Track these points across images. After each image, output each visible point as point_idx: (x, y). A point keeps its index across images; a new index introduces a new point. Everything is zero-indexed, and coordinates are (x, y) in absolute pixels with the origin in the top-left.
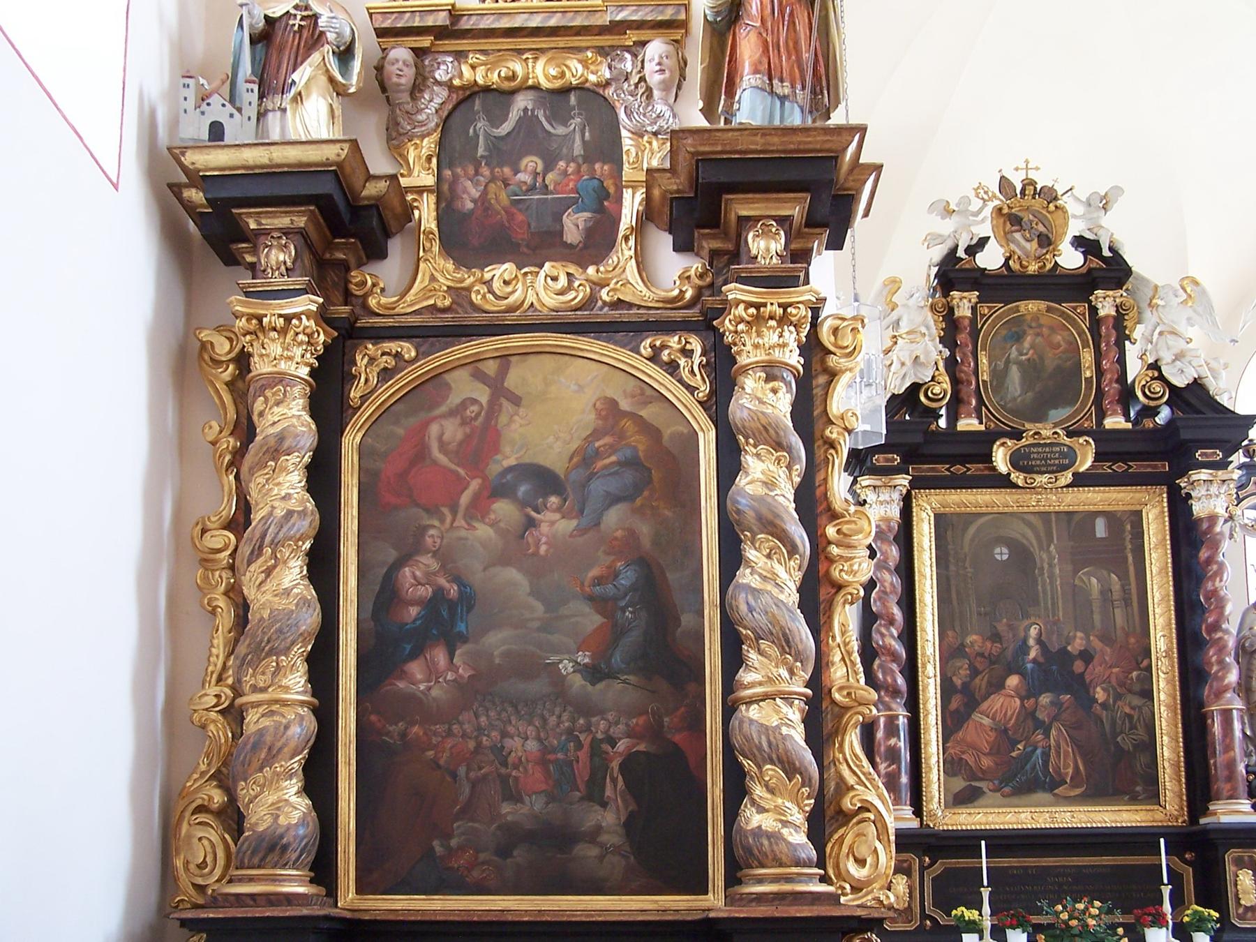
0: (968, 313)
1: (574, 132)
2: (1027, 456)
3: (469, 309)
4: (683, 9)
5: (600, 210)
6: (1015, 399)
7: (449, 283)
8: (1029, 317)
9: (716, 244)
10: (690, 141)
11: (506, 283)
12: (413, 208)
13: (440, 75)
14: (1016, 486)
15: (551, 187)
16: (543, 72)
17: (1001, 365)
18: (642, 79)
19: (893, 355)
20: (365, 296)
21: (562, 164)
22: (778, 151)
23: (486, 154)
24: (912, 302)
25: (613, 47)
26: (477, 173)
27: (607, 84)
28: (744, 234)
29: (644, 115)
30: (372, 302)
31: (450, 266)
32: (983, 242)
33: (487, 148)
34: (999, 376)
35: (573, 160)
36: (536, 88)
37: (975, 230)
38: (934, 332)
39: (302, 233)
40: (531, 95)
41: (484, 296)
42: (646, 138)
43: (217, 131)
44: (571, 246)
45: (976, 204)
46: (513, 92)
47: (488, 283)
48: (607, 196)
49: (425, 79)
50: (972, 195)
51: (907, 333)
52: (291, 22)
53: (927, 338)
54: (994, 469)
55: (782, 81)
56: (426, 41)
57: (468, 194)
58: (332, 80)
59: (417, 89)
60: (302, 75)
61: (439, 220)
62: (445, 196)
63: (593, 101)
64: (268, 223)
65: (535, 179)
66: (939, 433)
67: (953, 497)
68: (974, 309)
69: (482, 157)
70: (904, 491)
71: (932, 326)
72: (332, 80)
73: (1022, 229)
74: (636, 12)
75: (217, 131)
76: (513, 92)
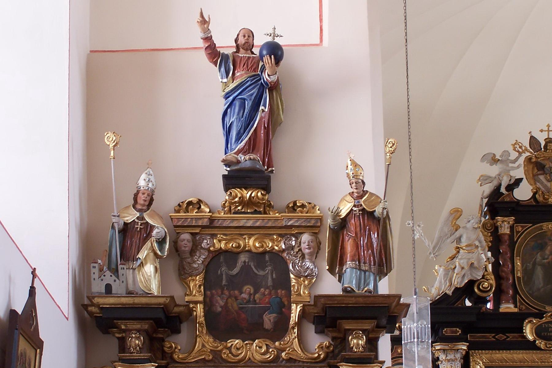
0: (507, 231)
1: (267, 274)
2: (547, 330)
3: (221, 361)
4: (319, 221)
5: (280, 313)
6: (539, 289)
7: (211, 348)
8: (549, 233)
9: (335, 334)
10: (322, 300)
11: (238, 349)
12: (193, 311)
13: (204, 245)
14: (539, 349)
15: (258, 301)
16: (252, 243)
17: (530, 266)
18: (300, 250)
19: (457, 262)
20: (172, 354)
21: (262, 290)
22: (362, 304)
23: (227, 284)
24: (469, 225)
25: (286, 234)
26: (222, 293)
27: (284, 251)
28: (347, 337)
29: (301, 266)
30: (176, 357)
31: (211, 340)
32: (518, 182)
33: (227, 281)
34: (528, 274)
35: (267, 288)
36: (250, 251)
37: (512, 173)
38: (484, 244)
39: (146, 331)
40: (247, 255)
41: (228, 355)
42: (302, 279)
43: (108, 288)
44: (267, 330)
45: (514, 155)
46: (239, 253)
47: (229, 349)
48: (284, 306)
49: (197, 246)
50: (510, 149)
51: (466, 246)
52: (136, 226)
53: (480, 248)
54: (525, 337)
55: (365, 263)
56: (197, 231)
57: (219, 303)
58: (156, 254)
59: (192, 252)
60: (142, 255)
61: (205, 316)
62: (208, 304)
63: (277, 260)
64: (130, 327)
65: (250, 297)
66: (488, 313)
67: (498, 355)
68: (512, 228)
69: (225, 285)
70: (464, 353)
71: (481, 239)
72: (156, 254)
73: (544, 173)
74: (297, 221)
75: (108, 288)
76: (239, 253)
